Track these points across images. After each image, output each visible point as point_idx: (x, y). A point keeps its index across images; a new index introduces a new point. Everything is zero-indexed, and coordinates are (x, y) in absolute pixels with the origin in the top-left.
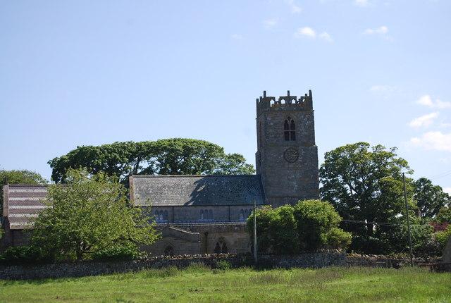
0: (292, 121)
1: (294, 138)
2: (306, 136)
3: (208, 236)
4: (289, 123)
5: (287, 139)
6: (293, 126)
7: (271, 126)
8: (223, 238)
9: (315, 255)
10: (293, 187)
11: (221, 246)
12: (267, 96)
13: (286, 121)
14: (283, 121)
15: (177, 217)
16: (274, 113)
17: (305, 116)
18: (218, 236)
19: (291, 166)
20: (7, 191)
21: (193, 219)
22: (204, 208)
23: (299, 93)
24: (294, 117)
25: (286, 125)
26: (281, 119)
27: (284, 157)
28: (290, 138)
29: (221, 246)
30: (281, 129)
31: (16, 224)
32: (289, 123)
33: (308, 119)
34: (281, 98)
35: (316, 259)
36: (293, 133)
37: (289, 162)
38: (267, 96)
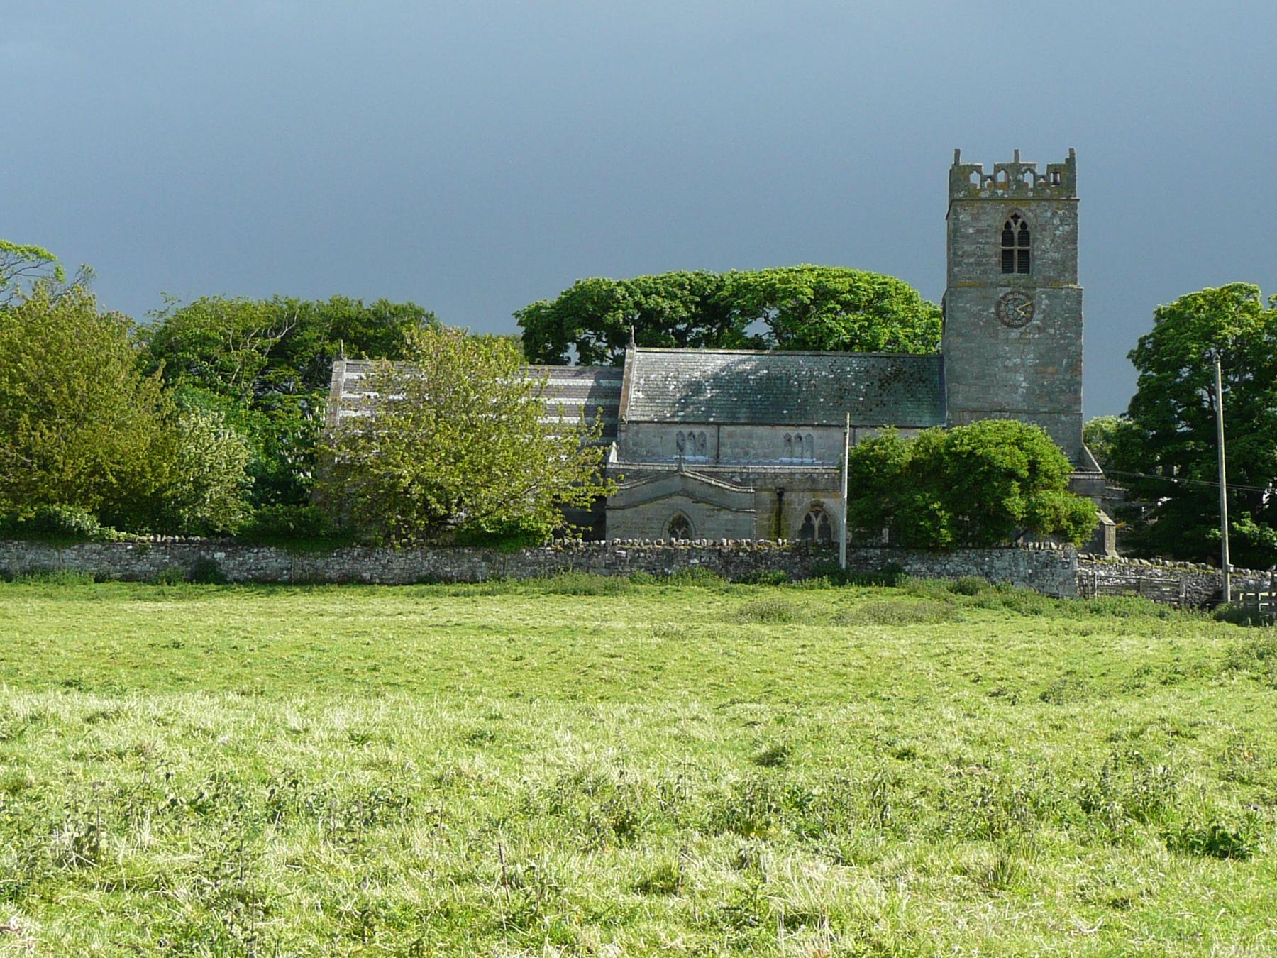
0: (1024, 225)
1: (1025, 267)
2: (1054, 261)
3: (785, 498)
4: (1016, 229)
5: (1007, 268)
6: (1025, 236)
7: (967, 236)
8: (820, 505)
9: (996, 553)
10: (1015, 387)
11: (817, 522)
12: (962, 162)
13: (1008, 225)
14: (1000, 224)
15: (725, 450)
16: (978, 204)
17: (1054, 214)
18: (808, 499)
19: (1015, 334)
20: (340, 374)
21: (766, 456)
22: (793, 432)
23: (1041, 158)
24: (1029, 214)
25: (1007, 237)
26: (996, 218)
27: (998, 313)
28: (1016, 268)
29: (817, 522)
30: (994, 245)
31: (579, 382)
32: (1016, 229)
33: (1062, 220)
34: (998, 168)
35: (997, 564)
36: (1025, 255)
37: (1009, 326)
38: (962, 162)
